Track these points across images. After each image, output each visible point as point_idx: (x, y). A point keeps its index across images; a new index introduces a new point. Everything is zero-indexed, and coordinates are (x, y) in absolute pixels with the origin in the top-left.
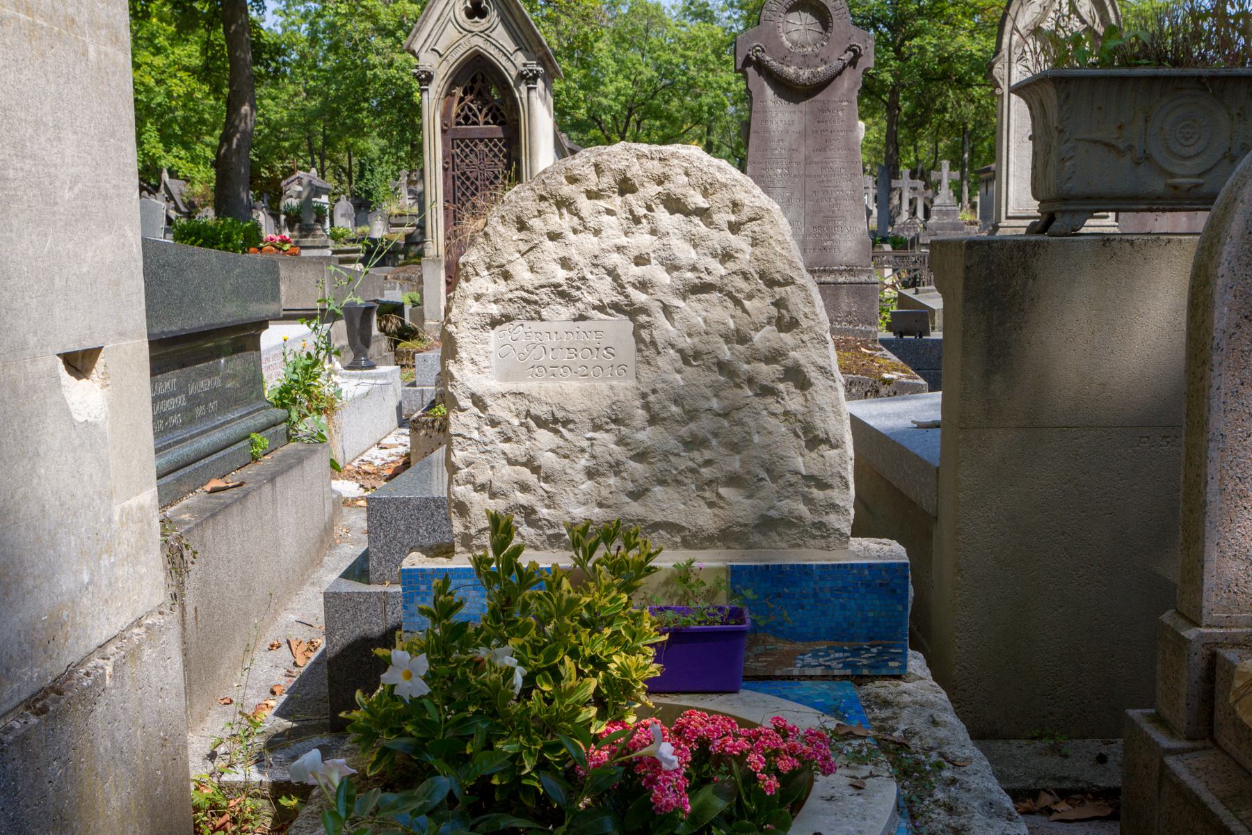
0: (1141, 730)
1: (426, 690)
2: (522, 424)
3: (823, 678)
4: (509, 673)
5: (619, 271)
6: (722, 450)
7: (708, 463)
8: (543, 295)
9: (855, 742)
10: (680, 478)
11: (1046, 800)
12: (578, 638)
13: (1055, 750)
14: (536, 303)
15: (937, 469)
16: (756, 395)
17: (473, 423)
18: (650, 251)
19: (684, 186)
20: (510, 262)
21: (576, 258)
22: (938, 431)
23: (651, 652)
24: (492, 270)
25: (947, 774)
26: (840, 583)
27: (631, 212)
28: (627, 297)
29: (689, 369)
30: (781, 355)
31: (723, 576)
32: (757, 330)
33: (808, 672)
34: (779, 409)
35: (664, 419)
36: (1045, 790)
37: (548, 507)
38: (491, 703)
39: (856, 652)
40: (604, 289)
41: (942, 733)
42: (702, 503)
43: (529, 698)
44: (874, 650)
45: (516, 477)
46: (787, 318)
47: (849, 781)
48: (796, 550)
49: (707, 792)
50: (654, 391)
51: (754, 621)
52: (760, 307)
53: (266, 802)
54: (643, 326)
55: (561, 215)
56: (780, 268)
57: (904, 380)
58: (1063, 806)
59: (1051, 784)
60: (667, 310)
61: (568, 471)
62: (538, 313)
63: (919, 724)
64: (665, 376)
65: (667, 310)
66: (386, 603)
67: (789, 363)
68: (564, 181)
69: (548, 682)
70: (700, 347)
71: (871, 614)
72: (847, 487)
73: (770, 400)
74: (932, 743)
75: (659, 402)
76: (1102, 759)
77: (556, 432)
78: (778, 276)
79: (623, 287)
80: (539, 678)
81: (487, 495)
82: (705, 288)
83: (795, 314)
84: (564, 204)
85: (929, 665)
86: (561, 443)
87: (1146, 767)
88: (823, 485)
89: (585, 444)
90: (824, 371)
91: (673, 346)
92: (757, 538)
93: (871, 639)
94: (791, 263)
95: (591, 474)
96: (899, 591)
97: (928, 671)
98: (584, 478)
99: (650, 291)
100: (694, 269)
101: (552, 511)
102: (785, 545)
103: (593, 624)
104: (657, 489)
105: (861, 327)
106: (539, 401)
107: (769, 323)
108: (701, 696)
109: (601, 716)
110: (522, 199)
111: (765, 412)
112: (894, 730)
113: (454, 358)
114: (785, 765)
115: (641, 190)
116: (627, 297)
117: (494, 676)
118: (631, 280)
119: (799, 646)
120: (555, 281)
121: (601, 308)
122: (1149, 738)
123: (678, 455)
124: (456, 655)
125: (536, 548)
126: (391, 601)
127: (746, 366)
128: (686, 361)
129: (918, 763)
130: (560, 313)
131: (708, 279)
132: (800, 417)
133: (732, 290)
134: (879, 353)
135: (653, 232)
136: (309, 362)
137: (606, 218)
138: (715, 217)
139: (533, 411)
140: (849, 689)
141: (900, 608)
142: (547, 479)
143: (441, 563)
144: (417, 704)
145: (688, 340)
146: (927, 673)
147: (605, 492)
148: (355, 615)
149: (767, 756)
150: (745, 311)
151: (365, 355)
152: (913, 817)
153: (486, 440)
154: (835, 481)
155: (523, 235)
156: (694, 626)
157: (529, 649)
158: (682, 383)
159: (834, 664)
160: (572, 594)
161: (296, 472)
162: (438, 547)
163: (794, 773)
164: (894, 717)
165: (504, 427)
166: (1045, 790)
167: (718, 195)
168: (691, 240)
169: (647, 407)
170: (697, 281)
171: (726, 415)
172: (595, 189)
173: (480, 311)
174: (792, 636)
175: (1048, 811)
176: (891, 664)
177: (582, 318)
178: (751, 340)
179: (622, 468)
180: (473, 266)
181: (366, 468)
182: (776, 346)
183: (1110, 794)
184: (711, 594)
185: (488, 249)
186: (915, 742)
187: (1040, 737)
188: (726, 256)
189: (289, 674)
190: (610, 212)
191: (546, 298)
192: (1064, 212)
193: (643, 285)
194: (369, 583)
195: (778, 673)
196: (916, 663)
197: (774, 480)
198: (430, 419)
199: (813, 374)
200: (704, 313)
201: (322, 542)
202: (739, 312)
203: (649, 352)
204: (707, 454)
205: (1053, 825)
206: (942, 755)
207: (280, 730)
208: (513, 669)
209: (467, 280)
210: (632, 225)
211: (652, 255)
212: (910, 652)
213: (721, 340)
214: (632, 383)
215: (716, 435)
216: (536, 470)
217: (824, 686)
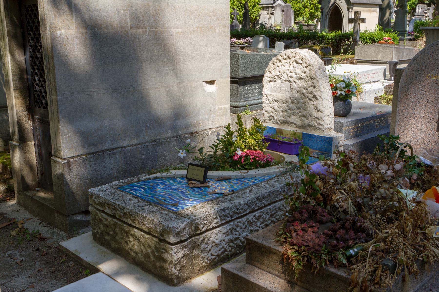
7: (300, 112)
8: (276, 77)
17: (266, 99)
21: (281, 71)
33: (315, 156)
40: (285, 77)
70: (300, 90)
73: (311, 101)
82: (301, 78)
84: (280, 61)
88: (319, 120)
92: (308, 128)
95: (283, 111)
104: (293, 116)
119: (313, 150)
121: (285, 81)
130: (279, 81)
131: (301, 77)
177: (282, 82)
199: (318, 97)
204: (300, 110)
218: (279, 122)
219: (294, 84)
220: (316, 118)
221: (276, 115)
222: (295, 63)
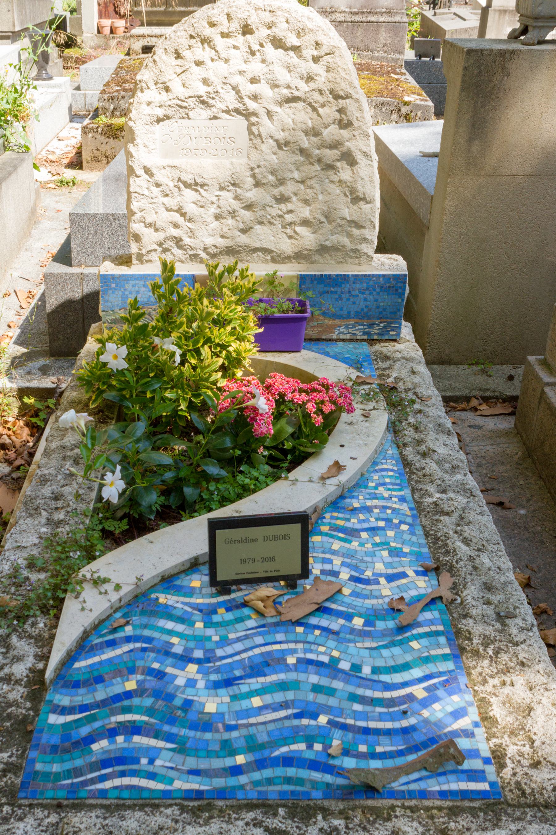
0: (534, 370)
1: (126, 366)
2: (175, 186)
3: (351, 340)
4: (173, 354)
5: (240, 88)
6: (300, 204)
7: (290, 212)
8: (191, 103)
9: (366, 387)
10: (272, 221)
11: (474, 403)
12: (212, 332)
13: (484, 372)
14: (186, 108)
15: (432, 197)
16: (322, 169)
17: (145, 184)
18: (260, 74)
19: (285, 30)
20: (170, 80)
21: (212, 78)
22: (436, 160)
23: (253, 339)
24: (158, 86)
25: (417, 406)
26: (365, 286)
27: (250, 47)
28: (244, 105)
29: (281, 152)
30: (340, 144)
31: (295, 281)
32: (326, 128)
33: (342, 337)
34: (335, 178)
35: (264, 184)
36: (475, 397)
37: (190, 237)
38: (161, 372)
39: (371, 326)
40: (229, 99)
41: (417, 379)
42: (285, 236)
43: (184, 366)
44: (382, 325)
45: (171, 219)
46: (345, 121)
47: (362, 412)
48: (340, 265)
49: (283, 422)
50: (259, 167)
51: (312, 313)
52: (329, 112)
53: (14, 399)
54: (253, 124)
55: (204, 48)
56: (343, 87)
57: (418, 102)
58: (484, 407)
59: (479, 393)
60: (269, 114)
61: (203, 216)
62: (187, 114)
63: (404, 374)
64: (266, 157)
65: (269, 114)
66: (83, 280)
67: (344, 149)
68: (207, 26)
69: (194, 357)
70: (289, 138)
71: (382, 304)
72: (374, 227)
73: (331, 172)
74: (410, 386)
75: (262, 173)
76: (511, 378)
77: (197, 191)
78: (341, 93)
79: (242, 98)
80: (189, 354)
81: (152, 230)
82: (295, 99)
83: (350, 118)
84: (205, 41)
85: (414, 332)
86: (199, 198)
87: (533, 391)
88: (359, 226)
89: (214, 199)
90: (365, 154)
91: (272, 137)
92: (317, 257)
93: (381, 318)
94: (350, 84)
95: (217, 217)
96: (400, 291)
97: (413, 336)
98: (213, 220)
99: (259, 101)
100: (288, 87)
101: (192, 240)
102: (333, 262)
103: (221, 322)
104: (258, 227)
105: (392, 56)
106: (186, 171)
107: (334, 123)
108: (278, 354)
109: (223, 377)
110: (179, 37)
111: (327, 180)
112: (389, 377)
113: (133, 143)
114: (327, 408)
115: (256, 32)
116: (244, 105)
117: (165, 357)
118: (248, 94)
119: (338, 322)
120: (198, 94)
121: (227, 112)
122: (537, 375)
123: (272, 206)
124: (141, 342)
125: (182, 262)
126: (86, 278)
127: (317, 152)
128: (279, 147)
129: (402, 400)
130: (200, 114)
131: (296, 94)
132: (349, 184)
133: (312, 101)
134: (404, 77)
135: (263, 61)
136: (16, 95)
137: (233, 51)
138: (304, 52)
139: (182, 178)
140: (366, 348)
141: (400, 300)
142: (190, 220)
143: (123, 270)
144: (121, 372)
145: (282, 133)
146: (412, 337)
147: (225, 229)
148: (63, 287)
149: (316, 404)
150: (319, 115)
151: (46, 70)
152: (395, 432)
153: (153, 196)
154: (367, 224)
155: (179, 62)
156: (277, 315)
157: (183, 339)
158: (276, 161)
159: (357, 333)
160: (210, 309)
161: (13, 177)
162: (121, 257)
163: (331, 413)
164: (390, 368)
165: (164, 188)
166: (475, 397)
167: (307, 37)
168: (288, 67)
169: (254, 176)
170: (290, 95)
171: (303, 182)
172: (227, 31)
173: (150, 113)
174: (334, 316)
175: (475, 409)
176: (391, 333)
177: (215, 118)
178: (321, 134)
179: (236, 214)
180: (146, 83)
181: (51, 157)
182: (337, 139)
183: (513, 399)
184: (287, 291)
185: (156, 71)
186: (401, 386)
187: (477, 364)
188: (310, 79)
189: (18, 314)
190: (235, 47)
191: (192, 105)
192: (535, 27)
193: (255, 97)
194: (71, 265)
195: (324, 337)
196: (406, 330)
197: (330, 222)
198: (95, 126)
199: (359, 157)
200: (293, 116)
201: (30, 220)
202: (315, 116)
203: (257, 141)
204: (290, 206)
205: (476, 418)
206: (415, 393)
207: (19, 354)
208: (175, 353)
209: (142, 91)
210: (250, 56)
211: (262, 77)
212: (404, 322)
213: (303, 134)
214: (245, 160)
215: (296, 194)
216: (183, 215)
217: (351, 346)
218: (203, 255)
219: (264, 119)
220: (353, 222)
221: (192, 234)
222: (269, 49)
